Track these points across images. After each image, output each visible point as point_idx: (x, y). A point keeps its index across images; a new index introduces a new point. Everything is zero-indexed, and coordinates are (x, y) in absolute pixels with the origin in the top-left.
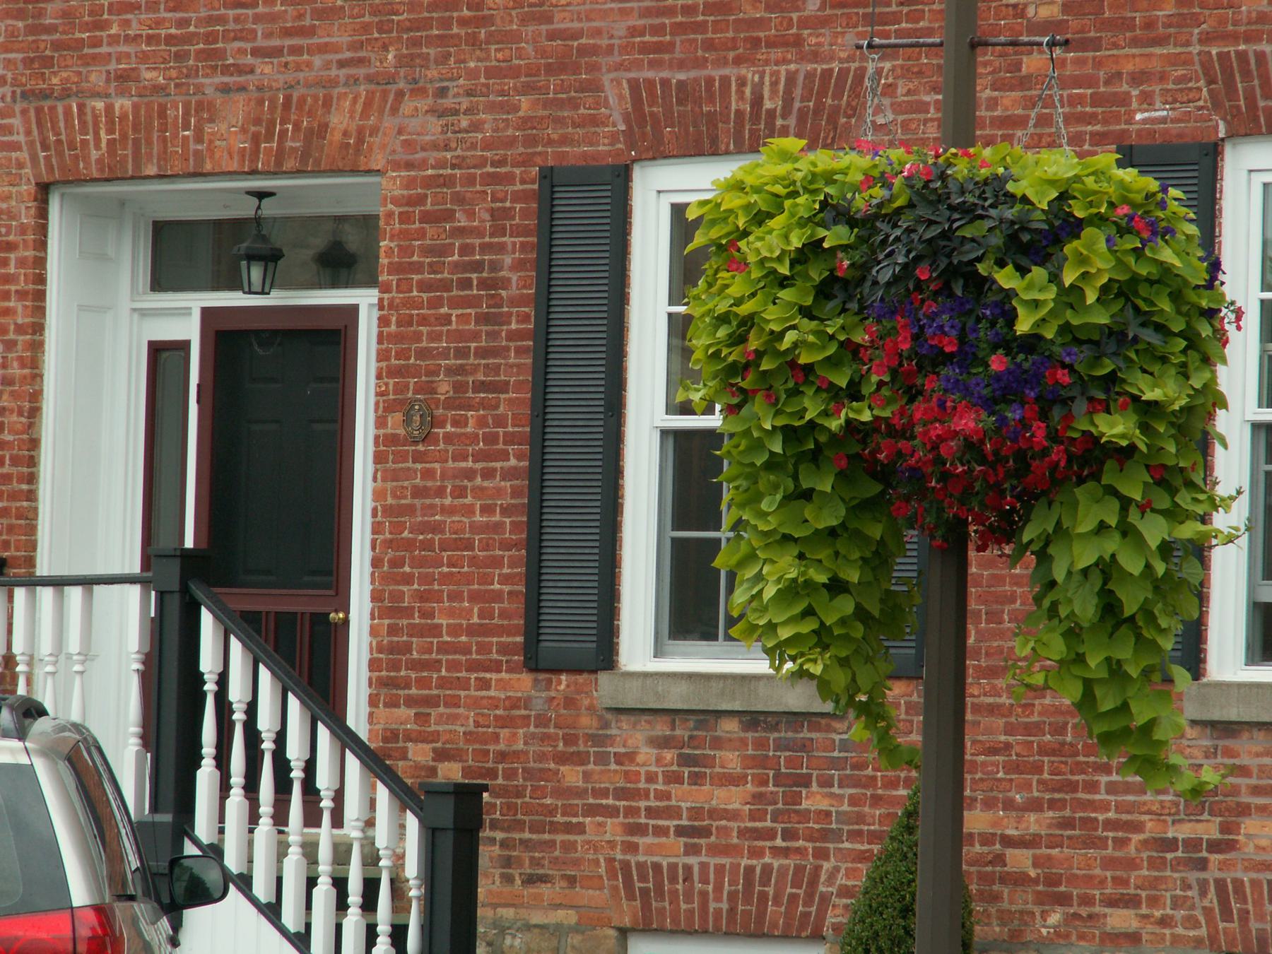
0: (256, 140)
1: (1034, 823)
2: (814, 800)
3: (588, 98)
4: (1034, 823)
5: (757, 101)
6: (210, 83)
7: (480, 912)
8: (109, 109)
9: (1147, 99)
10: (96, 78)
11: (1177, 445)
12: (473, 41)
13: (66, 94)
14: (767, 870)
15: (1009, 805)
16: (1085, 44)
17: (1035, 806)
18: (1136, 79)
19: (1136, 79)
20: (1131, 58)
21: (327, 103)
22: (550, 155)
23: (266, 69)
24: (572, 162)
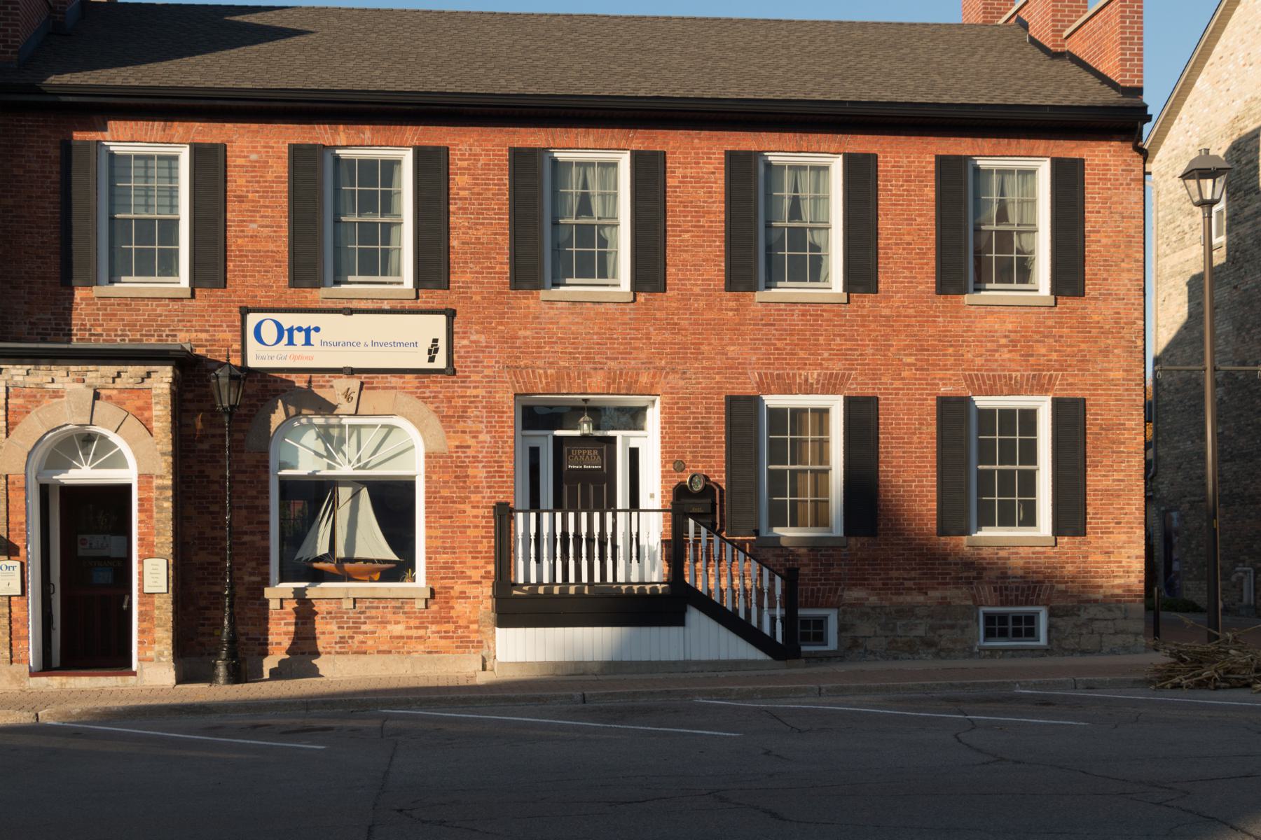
0: (609, 384)
1: (913, 574)
2: (835, 570)
3: (743, 377)
4: (913, 574)
5: (806, 380)
6: (588, 367)
7: (722, 207)
8: (545, 373)
9: (945, 385)
10: (540, 363)
11: (235, 366)
12: (696, 359)
13: (527, 367)
14: (819, 590)
15: (905, 569)
16: (922, 370)
17: (914, 569)
18: (941, 379)
19: (941, 379)
20: (940, 374)
21: (638, 374)
22: (729, 392)
23: (612, 364)
24: (669, 528)
